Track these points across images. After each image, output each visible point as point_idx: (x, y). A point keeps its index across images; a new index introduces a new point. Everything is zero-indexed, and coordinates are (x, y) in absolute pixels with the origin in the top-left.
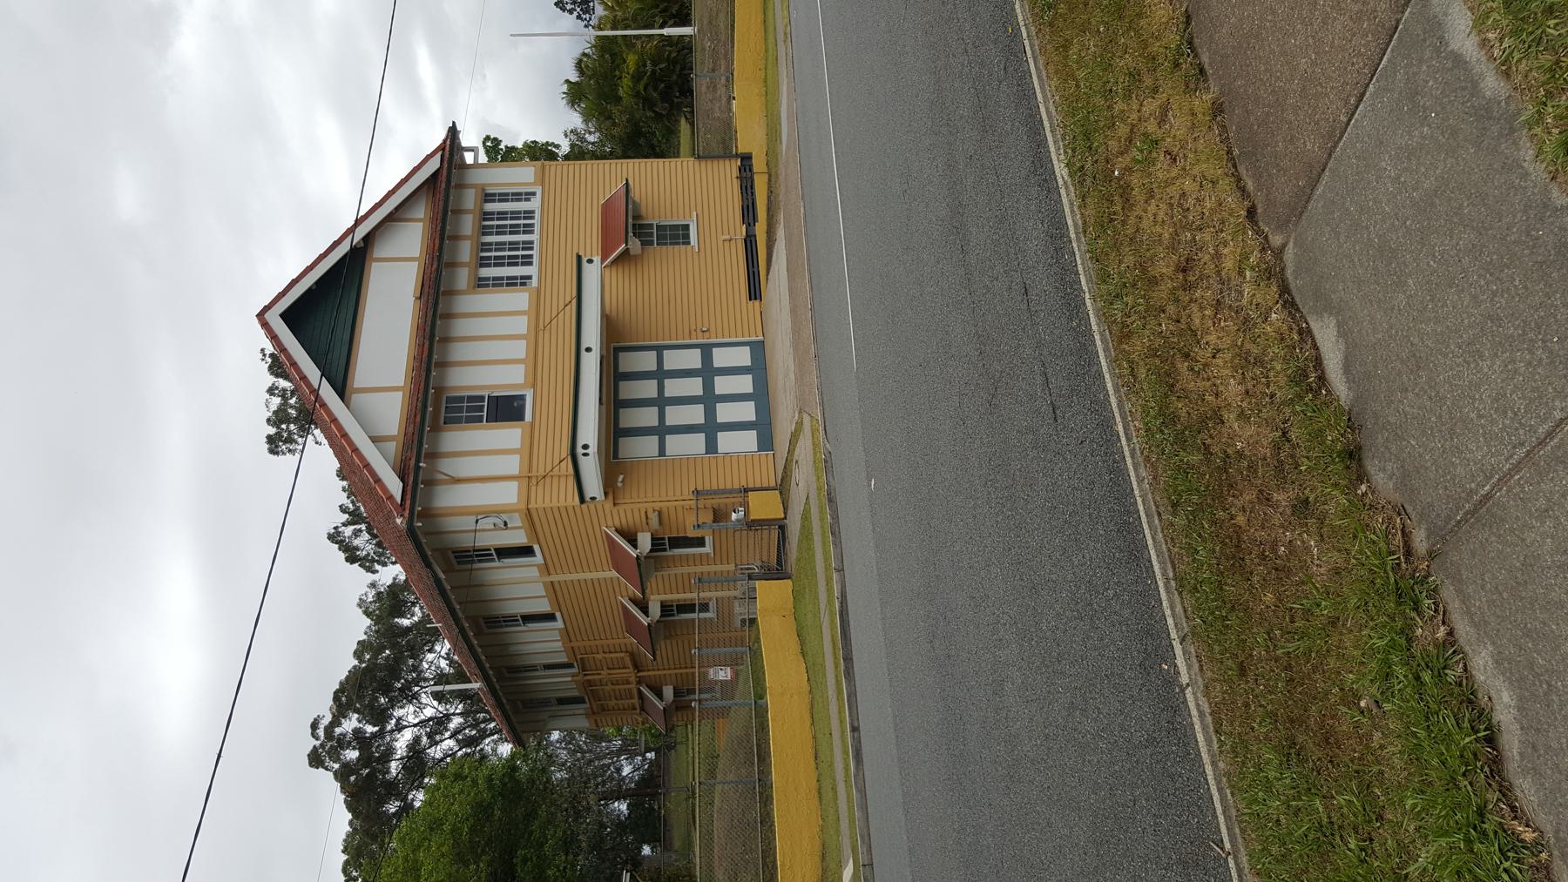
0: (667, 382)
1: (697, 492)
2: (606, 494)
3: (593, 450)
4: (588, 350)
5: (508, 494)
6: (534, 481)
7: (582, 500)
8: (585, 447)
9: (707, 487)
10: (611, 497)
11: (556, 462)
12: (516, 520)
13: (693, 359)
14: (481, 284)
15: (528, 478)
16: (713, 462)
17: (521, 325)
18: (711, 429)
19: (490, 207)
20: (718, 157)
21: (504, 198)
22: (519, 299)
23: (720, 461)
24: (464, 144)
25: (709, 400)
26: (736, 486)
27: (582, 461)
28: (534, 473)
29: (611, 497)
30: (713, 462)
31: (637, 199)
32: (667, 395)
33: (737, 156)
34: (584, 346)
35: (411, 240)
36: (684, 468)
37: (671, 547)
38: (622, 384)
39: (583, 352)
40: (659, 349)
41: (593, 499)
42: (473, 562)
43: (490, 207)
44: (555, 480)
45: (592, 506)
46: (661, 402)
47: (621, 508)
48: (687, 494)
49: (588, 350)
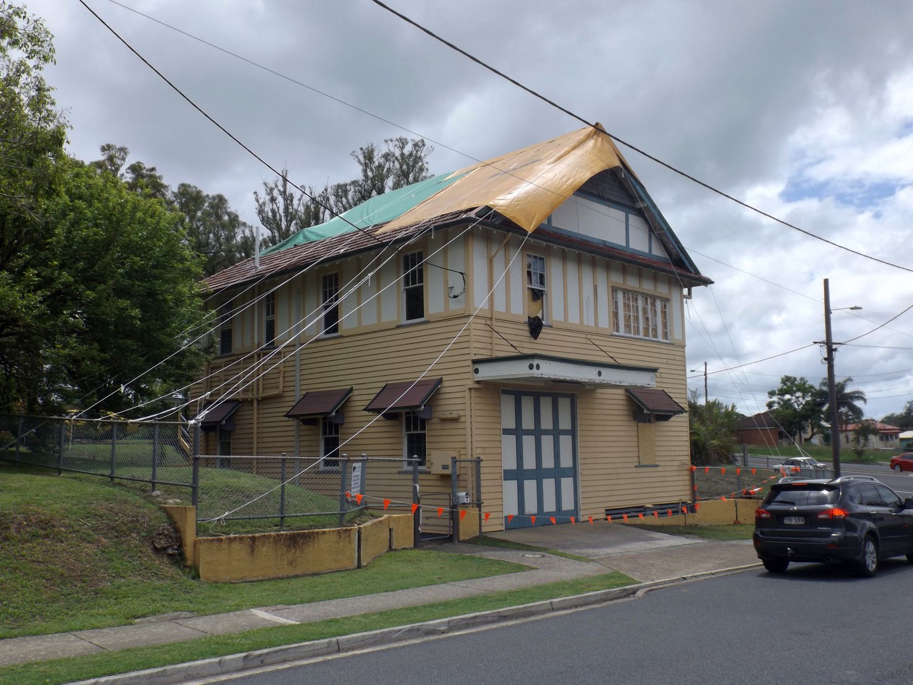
0: (570, 437)
1: (478, 461)
2: (478, 382)
3: (535, 373)
4: (600, 374)
5: (480, 302)
6: (489, 322)
7: (475, 362)
8: (538, 367)
9: (482, 470)
10: (477, 386)
11: (514, 344)
12: (456, 307)
13: (566, 462)
14: (614, 290)
15: (489, 319)
16: (497, 476)
17: (589, 322)
18: (518, 475)
19: (659, 304)
20: (693, 486)
21: (664, 313)
22: (605, 322)
23: (497, 483)
24: (693, 289)
25: (539, 474)
26: (483, 497)
27: (526, 363)
28: (495, 323)
29: (477, 386)
30: (497, 476)
31: (672, 419)
32: (561, 437)
33: (694, 499)
34: (604, 371)
35: (639, 242)
36: (264, 445)
37: (410, 437)
38: (532, 398)
39: (598, 369)
40: (573, 432)
41: (476, 371)
42: (325, 287)
43: (659, 304)
44: (488, 340)
45: (469, 369)
46: (538, 433)
47: (467, 394)
48: (477, 452)
49: (600, 374)
